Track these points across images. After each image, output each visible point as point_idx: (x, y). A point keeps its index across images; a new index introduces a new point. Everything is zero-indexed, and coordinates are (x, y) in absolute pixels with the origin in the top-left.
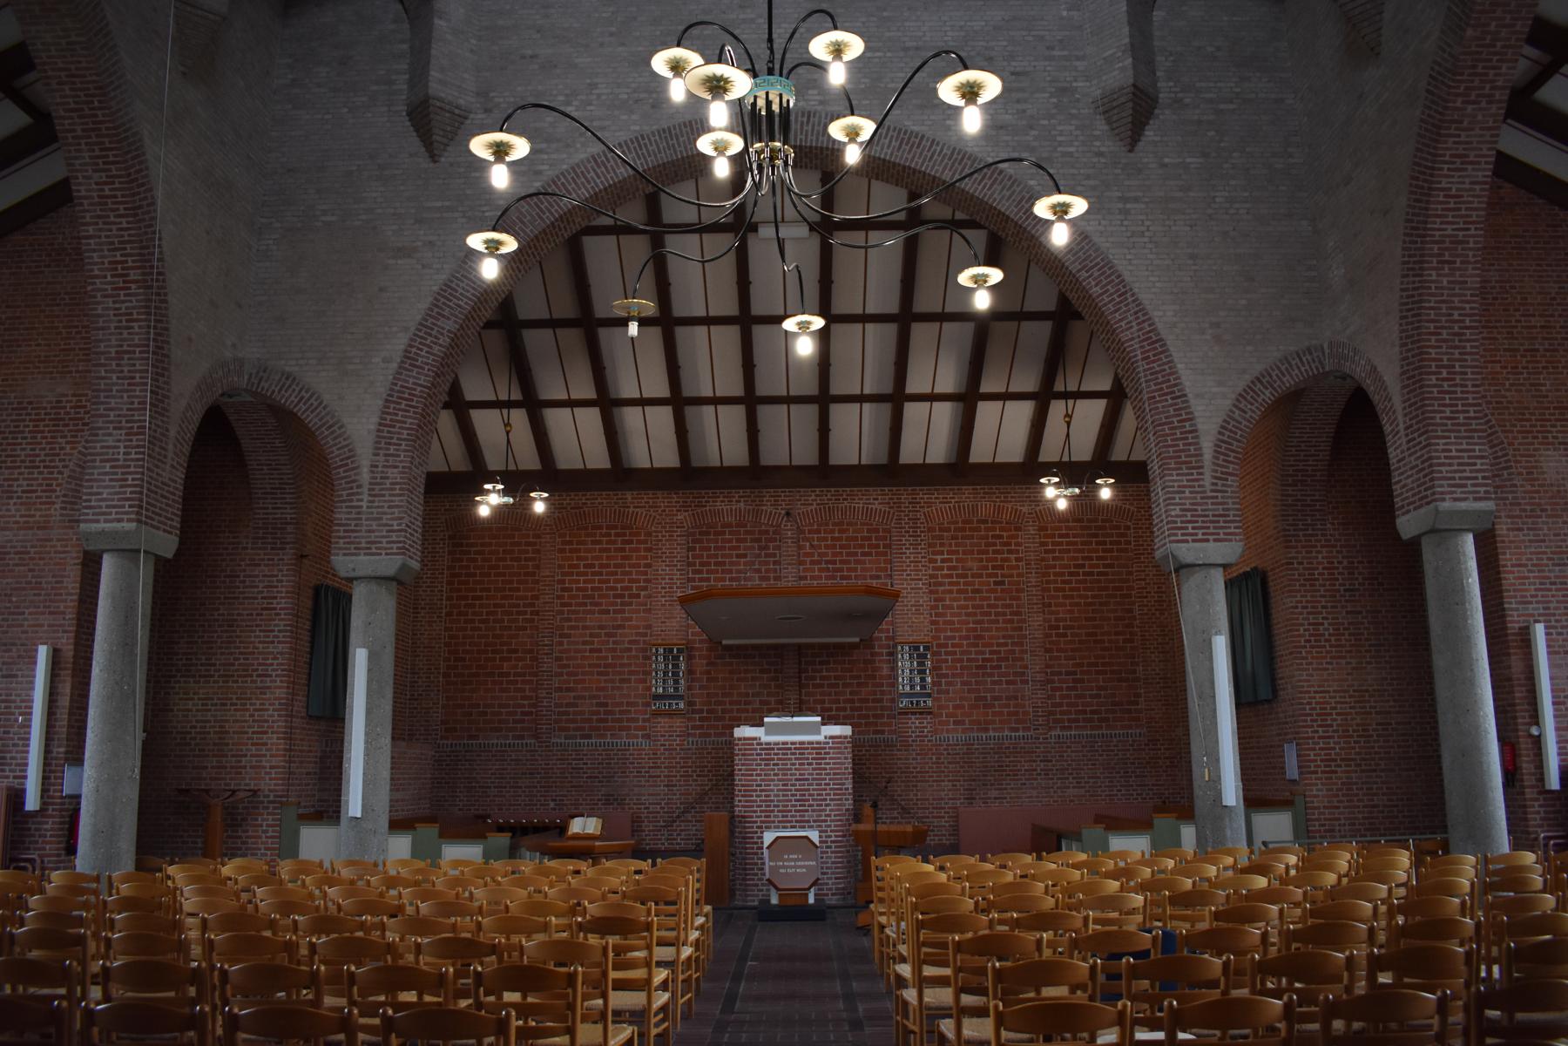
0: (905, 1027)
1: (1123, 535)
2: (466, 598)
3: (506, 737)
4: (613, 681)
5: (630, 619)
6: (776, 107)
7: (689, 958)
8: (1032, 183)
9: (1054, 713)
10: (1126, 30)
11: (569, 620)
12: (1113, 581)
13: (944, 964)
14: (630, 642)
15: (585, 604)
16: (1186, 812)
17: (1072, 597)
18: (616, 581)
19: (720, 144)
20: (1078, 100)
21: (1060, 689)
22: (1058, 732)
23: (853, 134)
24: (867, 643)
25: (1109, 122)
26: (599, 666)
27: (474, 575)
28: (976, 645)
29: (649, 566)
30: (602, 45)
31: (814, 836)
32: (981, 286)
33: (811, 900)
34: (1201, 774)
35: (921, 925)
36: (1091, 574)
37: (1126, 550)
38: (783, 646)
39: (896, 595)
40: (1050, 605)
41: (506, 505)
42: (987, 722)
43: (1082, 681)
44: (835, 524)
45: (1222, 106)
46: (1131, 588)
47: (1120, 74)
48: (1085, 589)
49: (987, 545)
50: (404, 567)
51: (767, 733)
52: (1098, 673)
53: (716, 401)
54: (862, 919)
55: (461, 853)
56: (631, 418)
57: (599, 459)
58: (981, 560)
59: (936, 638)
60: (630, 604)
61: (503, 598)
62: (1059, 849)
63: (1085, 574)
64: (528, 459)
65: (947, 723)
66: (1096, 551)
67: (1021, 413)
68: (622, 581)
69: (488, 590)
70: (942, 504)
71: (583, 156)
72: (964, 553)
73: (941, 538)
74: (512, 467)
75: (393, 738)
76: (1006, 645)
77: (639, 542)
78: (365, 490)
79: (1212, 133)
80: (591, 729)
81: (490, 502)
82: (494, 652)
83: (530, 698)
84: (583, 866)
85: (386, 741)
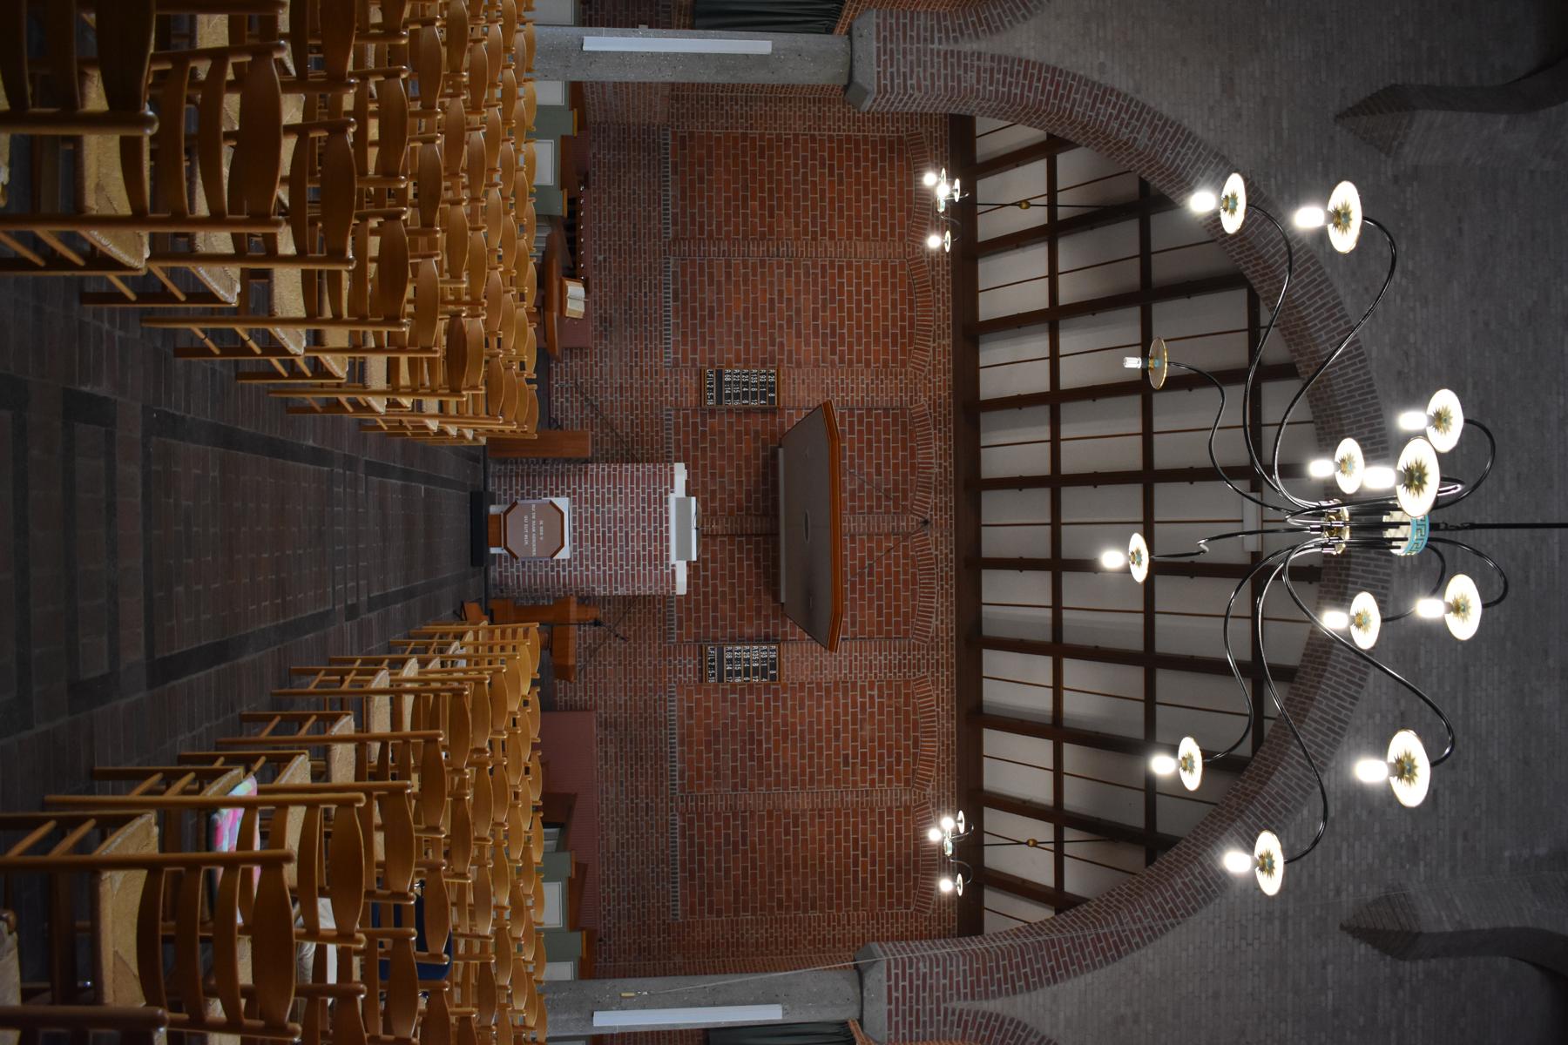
0: (348, 672)
1: (899, 902)
2: (831, 158)
3: (675, 206)
4: (738, 325)
5: (807, 344)
6: (1390, 533)
7: (426, 427)
8: (1305, 812)
9: (700, 819)
10: (1486, 926)
11: (807, 275)
12: (847, 888)
13: (414, 726)
14: (781, 344)
15: (824, 293)
16: (587, 971)
17: (830, 842)
18: (850, 328)
19: (1349, 468)
20: (1402, 867)
21: (727, 827)
22: (679, 823)
23: (1359, 621)
24: (780, 611)
25: (1376, 902)
26: (755, 309)
27: (858, 166)
28: (776, 733)
29: (868, 365)
30: (1474, 312)
31: (564, 554)
32: (1179, 765)
33: (493, 550)
34: (629, 988)
35: (458, 694)
36: (856, 864)
37: (882, 903)
38: (777, 516)
39: (831, 646)
40: (821, 817)
41: (936, 203)
42: (690, 744)
43: (736, 851)
44: (914, 575)
45: (1393, 1034)
46: (839, 909)
47: (1434, 917)
48: (838, 857)
49: (890, 748)
50: (865, 93)
51: (678, 500)
52: (745, 868)
53: (1055, 441)
54: (473, 609)
55: (544, 159)
56: (1038, 345)
57: (990, 307)
58: (872, 740)
59: (785, 688)
60: (824, 344)
61: (832, 201)
62: (546, 825)
63: (856, 857)
64: (990, 226)
65: (690, 699)
66: (882, 871)
67: (1039, 789)
68: (850, 335)
69: (841, 183)
70: (936, 697)
71: (1341, 292)
72: (881, 722)
73: (898, 695)
74: (980, 209)
75: (673, 84)
76: (777, 766)
77: (894, 353)
78: (952, 46)
79: (1362, 1020)
80: (685, 302)
81: (940, 186)
82: (771, 190)
83: (719, 232)
84: (529, 303)
85: (668, 76)
